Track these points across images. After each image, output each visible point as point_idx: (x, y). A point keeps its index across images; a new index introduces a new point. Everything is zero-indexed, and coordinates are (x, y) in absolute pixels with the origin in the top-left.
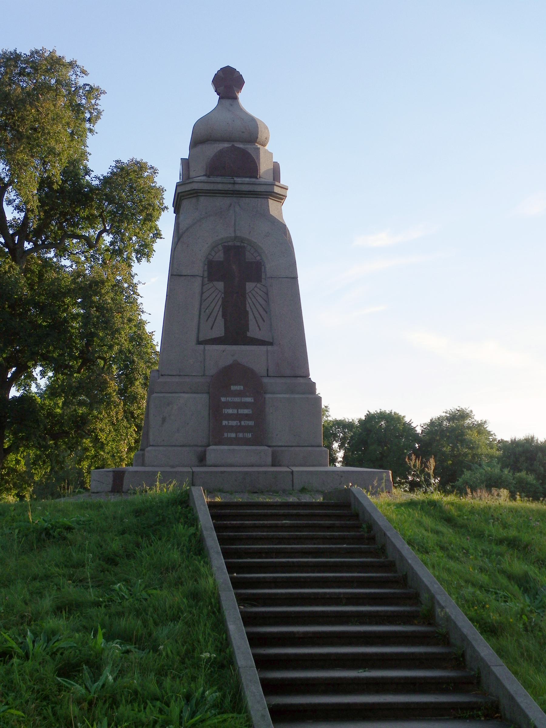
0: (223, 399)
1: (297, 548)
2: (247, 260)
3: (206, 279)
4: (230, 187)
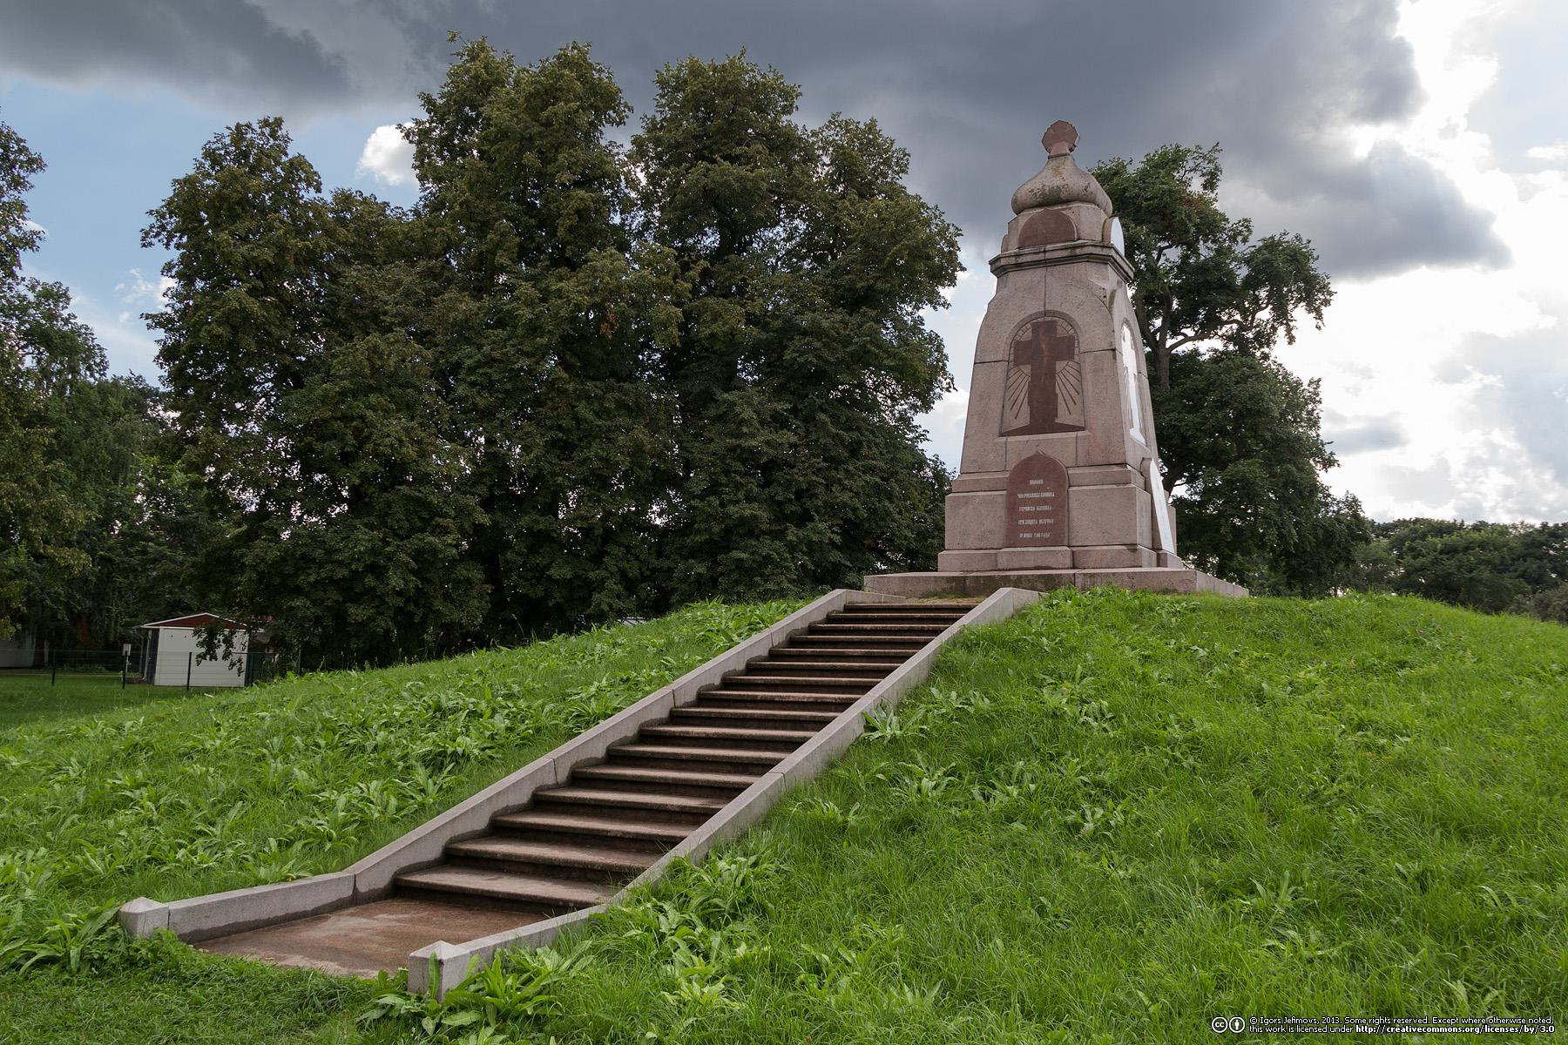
0: (1020, 496)
4: (1041, 256)
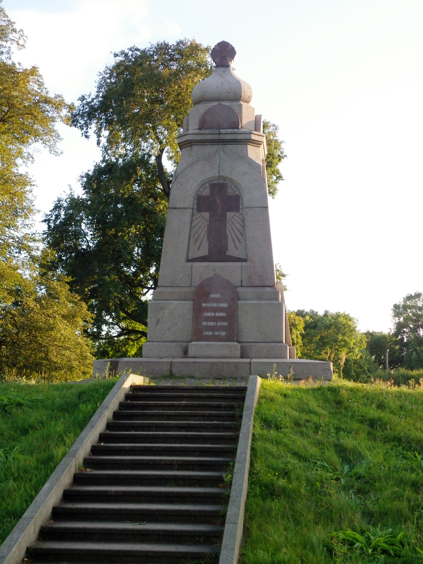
0: (204, 305)
1: (172, 424)
2: (228, 195)
3: (195, 211)
4: (216, 137)
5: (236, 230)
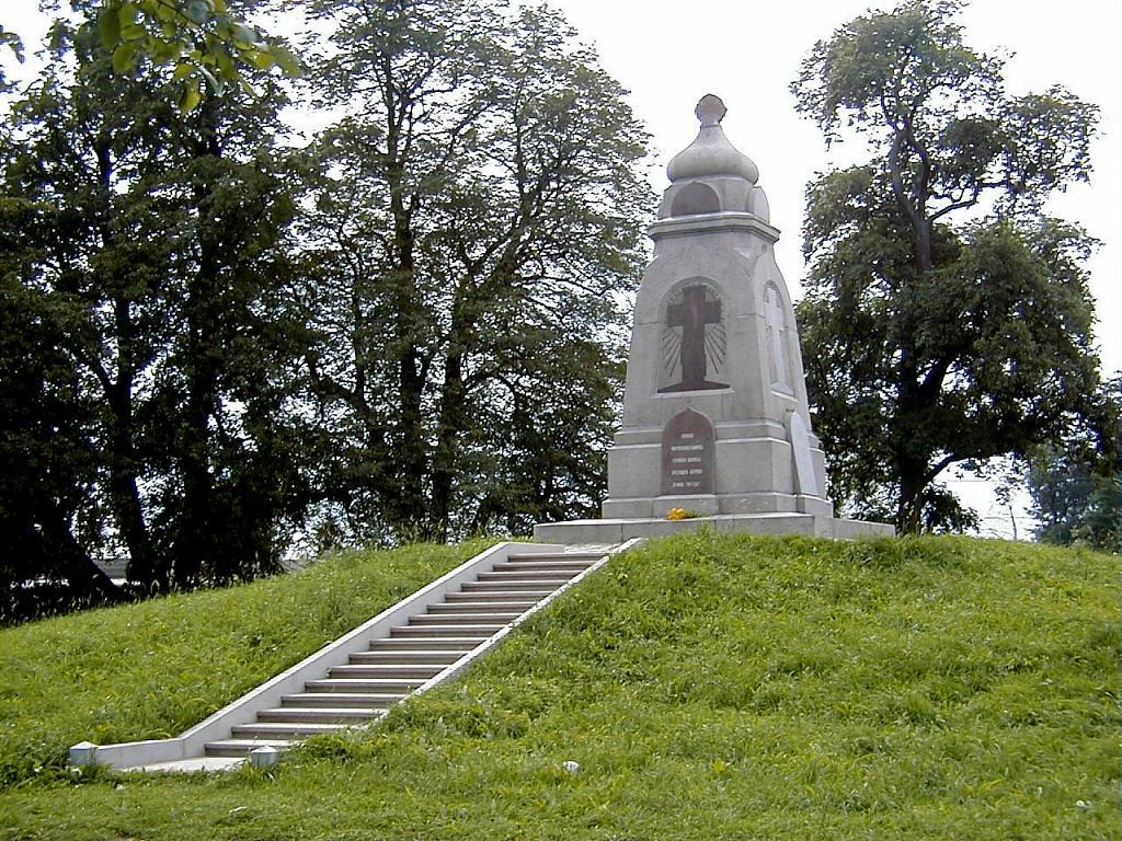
5: (716, 347)
